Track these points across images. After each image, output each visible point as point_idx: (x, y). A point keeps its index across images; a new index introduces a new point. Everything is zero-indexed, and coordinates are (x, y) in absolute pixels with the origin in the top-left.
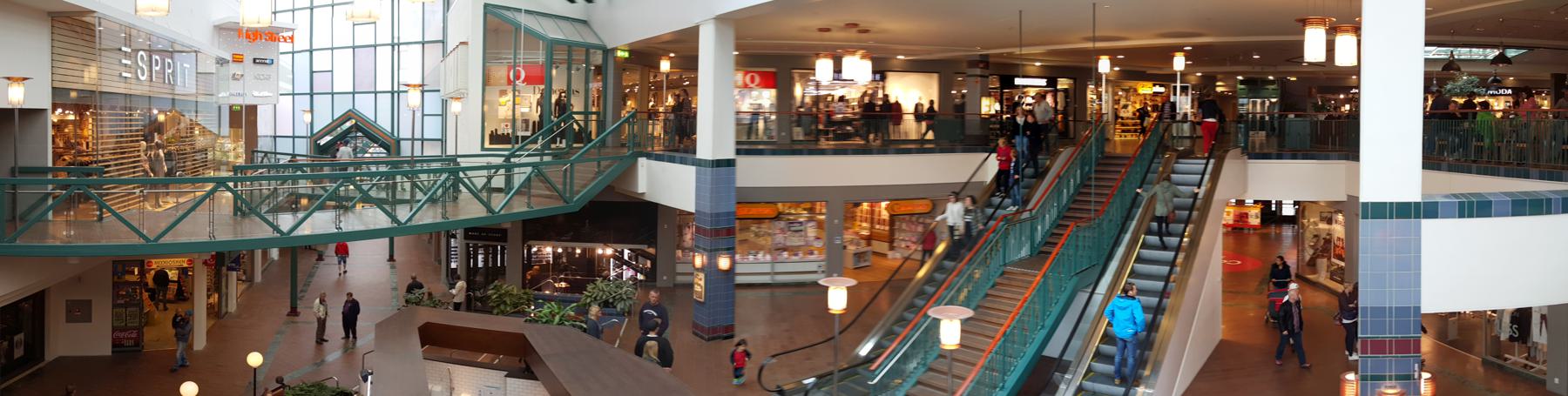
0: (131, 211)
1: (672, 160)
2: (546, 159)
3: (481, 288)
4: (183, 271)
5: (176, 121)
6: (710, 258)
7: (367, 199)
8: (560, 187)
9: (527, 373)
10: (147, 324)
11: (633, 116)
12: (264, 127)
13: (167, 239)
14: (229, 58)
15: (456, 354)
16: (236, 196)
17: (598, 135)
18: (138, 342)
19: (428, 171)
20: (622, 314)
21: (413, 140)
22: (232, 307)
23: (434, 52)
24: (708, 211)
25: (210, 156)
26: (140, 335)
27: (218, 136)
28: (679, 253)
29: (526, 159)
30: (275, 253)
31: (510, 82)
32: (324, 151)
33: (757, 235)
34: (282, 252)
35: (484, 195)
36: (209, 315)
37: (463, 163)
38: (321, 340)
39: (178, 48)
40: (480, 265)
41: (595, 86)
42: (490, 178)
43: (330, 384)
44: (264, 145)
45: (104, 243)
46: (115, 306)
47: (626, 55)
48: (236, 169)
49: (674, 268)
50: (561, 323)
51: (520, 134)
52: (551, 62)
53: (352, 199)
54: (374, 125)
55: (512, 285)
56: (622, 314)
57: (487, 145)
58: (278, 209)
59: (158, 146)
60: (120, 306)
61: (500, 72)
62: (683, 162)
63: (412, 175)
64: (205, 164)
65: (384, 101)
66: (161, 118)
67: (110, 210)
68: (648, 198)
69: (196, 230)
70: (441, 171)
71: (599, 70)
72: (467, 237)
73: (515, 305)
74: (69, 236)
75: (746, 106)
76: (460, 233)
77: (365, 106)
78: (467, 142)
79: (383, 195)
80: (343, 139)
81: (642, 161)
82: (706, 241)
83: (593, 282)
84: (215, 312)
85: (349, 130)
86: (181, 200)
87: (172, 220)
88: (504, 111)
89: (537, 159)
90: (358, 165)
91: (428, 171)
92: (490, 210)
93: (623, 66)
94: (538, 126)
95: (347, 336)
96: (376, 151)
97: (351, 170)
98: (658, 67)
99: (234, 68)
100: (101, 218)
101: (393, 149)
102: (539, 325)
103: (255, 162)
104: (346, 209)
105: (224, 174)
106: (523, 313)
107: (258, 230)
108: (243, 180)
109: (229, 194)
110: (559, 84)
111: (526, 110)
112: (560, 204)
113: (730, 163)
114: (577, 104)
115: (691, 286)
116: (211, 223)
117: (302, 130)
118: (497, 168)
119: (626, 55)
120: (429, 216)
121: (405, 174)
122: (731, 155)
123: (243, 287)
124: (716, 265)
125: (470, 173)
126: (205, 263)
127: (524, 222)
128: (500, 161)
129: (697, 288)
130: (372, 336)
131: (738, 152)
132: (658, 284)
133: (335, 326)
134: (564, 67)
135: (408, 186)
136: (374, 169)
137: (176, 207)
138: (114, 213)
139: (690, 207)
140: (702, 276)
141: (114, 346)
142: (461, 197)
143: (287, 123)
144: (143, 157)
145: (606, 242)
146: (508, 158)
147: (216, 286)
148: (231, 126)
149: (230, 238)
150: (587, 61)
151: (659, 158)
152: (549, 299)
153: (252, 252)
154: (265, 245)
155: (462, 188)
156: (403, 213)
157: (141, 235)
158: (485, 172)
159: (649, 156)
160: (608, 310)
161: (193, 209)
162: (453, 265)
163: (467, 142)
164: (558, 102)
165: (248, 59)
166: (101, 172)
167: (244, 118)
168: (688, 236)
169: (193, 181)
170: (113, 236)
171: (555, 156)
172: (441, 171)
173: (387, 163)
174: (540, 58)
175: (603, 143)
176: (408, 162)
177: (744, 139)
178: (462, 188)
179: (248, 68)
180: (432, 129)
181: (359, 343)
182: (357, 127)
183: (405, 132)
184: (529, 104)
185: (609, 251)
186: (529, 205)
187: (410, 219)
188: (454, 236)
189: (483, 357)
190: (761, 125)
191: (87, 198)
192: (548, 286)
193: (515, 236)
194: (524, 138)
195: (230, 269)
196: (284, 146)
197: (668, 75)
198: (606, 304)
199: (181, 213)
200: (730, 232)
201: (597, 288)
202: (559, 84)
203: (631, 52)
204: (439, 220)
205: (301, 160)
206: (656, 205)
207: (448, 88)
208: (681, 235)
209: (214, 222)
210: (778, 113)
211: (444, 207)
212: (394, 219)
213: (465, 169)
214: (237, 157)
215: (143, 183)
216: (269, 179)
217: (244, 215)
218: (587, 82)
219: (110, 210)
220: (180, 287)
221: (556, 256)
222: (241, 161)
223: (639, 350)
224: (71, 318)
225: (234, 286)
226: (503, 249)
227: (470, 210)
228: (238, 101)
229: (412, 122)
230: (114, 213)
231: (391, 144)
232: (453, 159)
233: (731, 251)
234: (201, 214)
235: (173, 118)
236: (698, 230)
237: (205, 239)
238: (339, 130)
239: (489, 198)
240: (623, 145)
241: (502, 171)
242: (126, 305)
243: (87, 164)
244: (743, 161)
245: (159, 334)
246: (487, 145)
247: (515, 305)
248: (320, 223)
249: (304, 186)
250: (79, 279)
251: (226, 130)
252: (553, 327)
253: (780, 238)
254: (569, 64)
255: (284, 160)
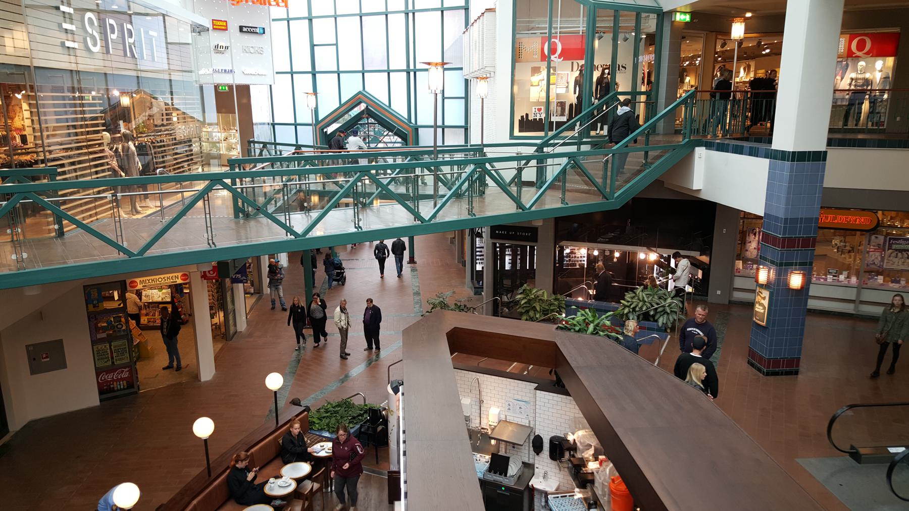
0: (103, 220)
1: (738, 150)
2: (585, 148)
3: (505, 290)
4: (177, 289)
5: (146, 103)
6: (778, 274)
7: (387, 195)
8: (599, 181)
9: (558, 386)
10: (139, 358)
11: (692, 96)
12: (260, 114)
13: (154, 251)
14: (207, 24)
15: (484, 362)
16: (236, 196)
17: (647, 119)
18: (132, 383)
19: (451, 163)
20: (663, 330)
21: (435, 127)
22: (242, 325)
23: (454, 21)
24: (781, 214)
25: (195, 148)
26: (133, 372)
27: (203, 123)
28: (739, 264)
29: (560, 153)
30: (283, 259)
31: (544, 57)
32: (332, 142)
33: (841, 250)
34: (291, 257)
35: (514, 189)
36: (214, 338)
37: (490, 153)
38: (344, 356)
39: (135, 8)
40: (508, 267)
41: (646, 59)
42: (520, 170)
43: (358, 401)
44: (261, 134)
45: (71, 263)
46: (94, 342)
47: (687, 18)
48: (232, 163)
49: (731, 282)
50: (595, 333)
51: (554, 119)
52: (594, 31)
53: (370, 195)
54: (388, 109)
55: (542, 290)
56: (663, 330)
57: (517, 133)
58: (286, 209)
59: (127, 138)
60: (102, 341)
61: (533, 45)
62: (753, 153)
63: (434, 168)
64: (190, 158)
65: (399, 80)
66: (126, 101)
67: (72, 220)
68: (705, 196)
69: (190, 237)
70: (461, 164)
71: (652, 39)
72: (493, 235)
73: (545, 312)
74: (19, 261)
75: (844, 84)
76: (486, 231)
77: (377, 88)
78: (494, 129)
79: (402, 190)
80: (351, 128)
81: (700, 152)
82: (775, 252)
83: (633, 290)
84: (222, 334)
85: (359, 117)
86: (166, 203)
87: (159, 227)
88: (537, 93)
89: (573, 149)
90: (372, 157)
91: (451, 163)
92: (520, 206)
93: (682, 33)
94: (576, 109)
95: (370, 347)
96: (391, 141)
97: (363, 162)
98: (728, 32)
99: (217, 38)
100: (61, 233)
101: (410, 139)
102: (571, 334)
103: (253, 157)
104: (364, 206)
105: (215, 169)
106: (554, 321)
107: (265, 232)
108: (241, 176)
109: (225, 193)
110: (602, 59)
111: (562, 91)
112: (598, 200)
113: (819, 157)
114: (623, 83)
115: (751, 305)
116: (209, 227)
117: (305, 117)
118: (528, 159)
119: (687, 18)
120: (454, 213)
121: (427, 166)
122: (821, 146)
123: (251, 301)
124: (787, 284)
125: (498, 165)
126: (204, 276)
127: (557, 220)
128: (531, 150)
129: (758, 309)
130: (399, 343)
131: (830, 143)
132: (711, 299)
133: (357, 334)
134: (609, 37)
135: (430, 179)
136: (390, 160)
137: (162, 210)
138: (79, 224)
139: (759, 210)
140: (766, 294)
141: (101, 392)
142: (487, 191)
143: (287, 110)
144: (108, 152)
145: (650, 245)
146: (540, 148)
147: (221, 302)
148: (219, 110)
149: (232, 243)
150: (637, 29)
151: (722, 148)
152: (582, 306)
153: (258, 259)
154: (273, 248)
155: (488, 180)
156: (426, 210)
157: (120, 249)
158: (514, 164)
159: (709, 146)
160: (647, 324)
161: (183, 213)
162: (479, 267)
163: (494, 129)
164: (600, 80)
165: (233, 27)
166: (52, 174)
167: (233, 101)
168: (753, 245)
169: (179, 180)
170: (81, 253)
171: (594, 145)
172: (461, 164)
173: (405, 155)
174: (580, 25)
175: (653, 129)
176: (429, 153)
177: (840, 125)
178: (488, 180)
179: (232, 38)
180: (454, 114)
181: (383, 353)
182: (368, 113)
183: (425, 117)
184: (565, 84)
185: (653, 257)
186: (563, 201)
187: (434, 216)
188: (480, 235)
189: (514, 367)
190: (866, 106)
191: (36, 209)
192: (581, 292)
193: (546, 235)
194: (559, 124)
195: (235, 281)
196: (285, 135)
197: (740, 42)
198: (645, 317)
199: (168, 219)
200: (809, 243)
201: (639, 297)
202: (602, 59)
203: (693, 14)
204: (465, 216)
205: (308, 152)
206: (714, 204)
207: (472, 66)
208: (743, 242)
209: (210, 226)
210: (893, 91)
211: (471, 203)
212: (417, 216)
213: (492, 161)
214: (230, 148)
215: (113, 186)
216: (273, 174)
217: (247, 216)
218: (636, 55)
219: (72, 220)
220: (175, 308)
221: (591, 260)
222: (236, 153)
223: (681, 370)
224: (35, 369)
225: (242, 300)
226: (532, 248)
227: (498, 205)
228: (227, 79)
229: (428, 105)
230: (79, 224)
231: (408, 133)
232: (479, 149)
233: (806, 267)
234: (196, 217)
235: (142, 102)
236: (766, 238)
237: (204, 247)
238: (347, 118)
239: (519, 192)
240: (677, 132)
241: (533, 163)
242: (109, 340)
243: (30, 164)
244: (836, 156)
245: (154, 370)
246: (517, 133)
247: (545, 312)
248: (337, 222)
249: (315, 181)
250: (40, 315)
251: (212, 115)
252: (587, 336)
253: (874, 257)
254: (615, 32)
255: (287, 152)
